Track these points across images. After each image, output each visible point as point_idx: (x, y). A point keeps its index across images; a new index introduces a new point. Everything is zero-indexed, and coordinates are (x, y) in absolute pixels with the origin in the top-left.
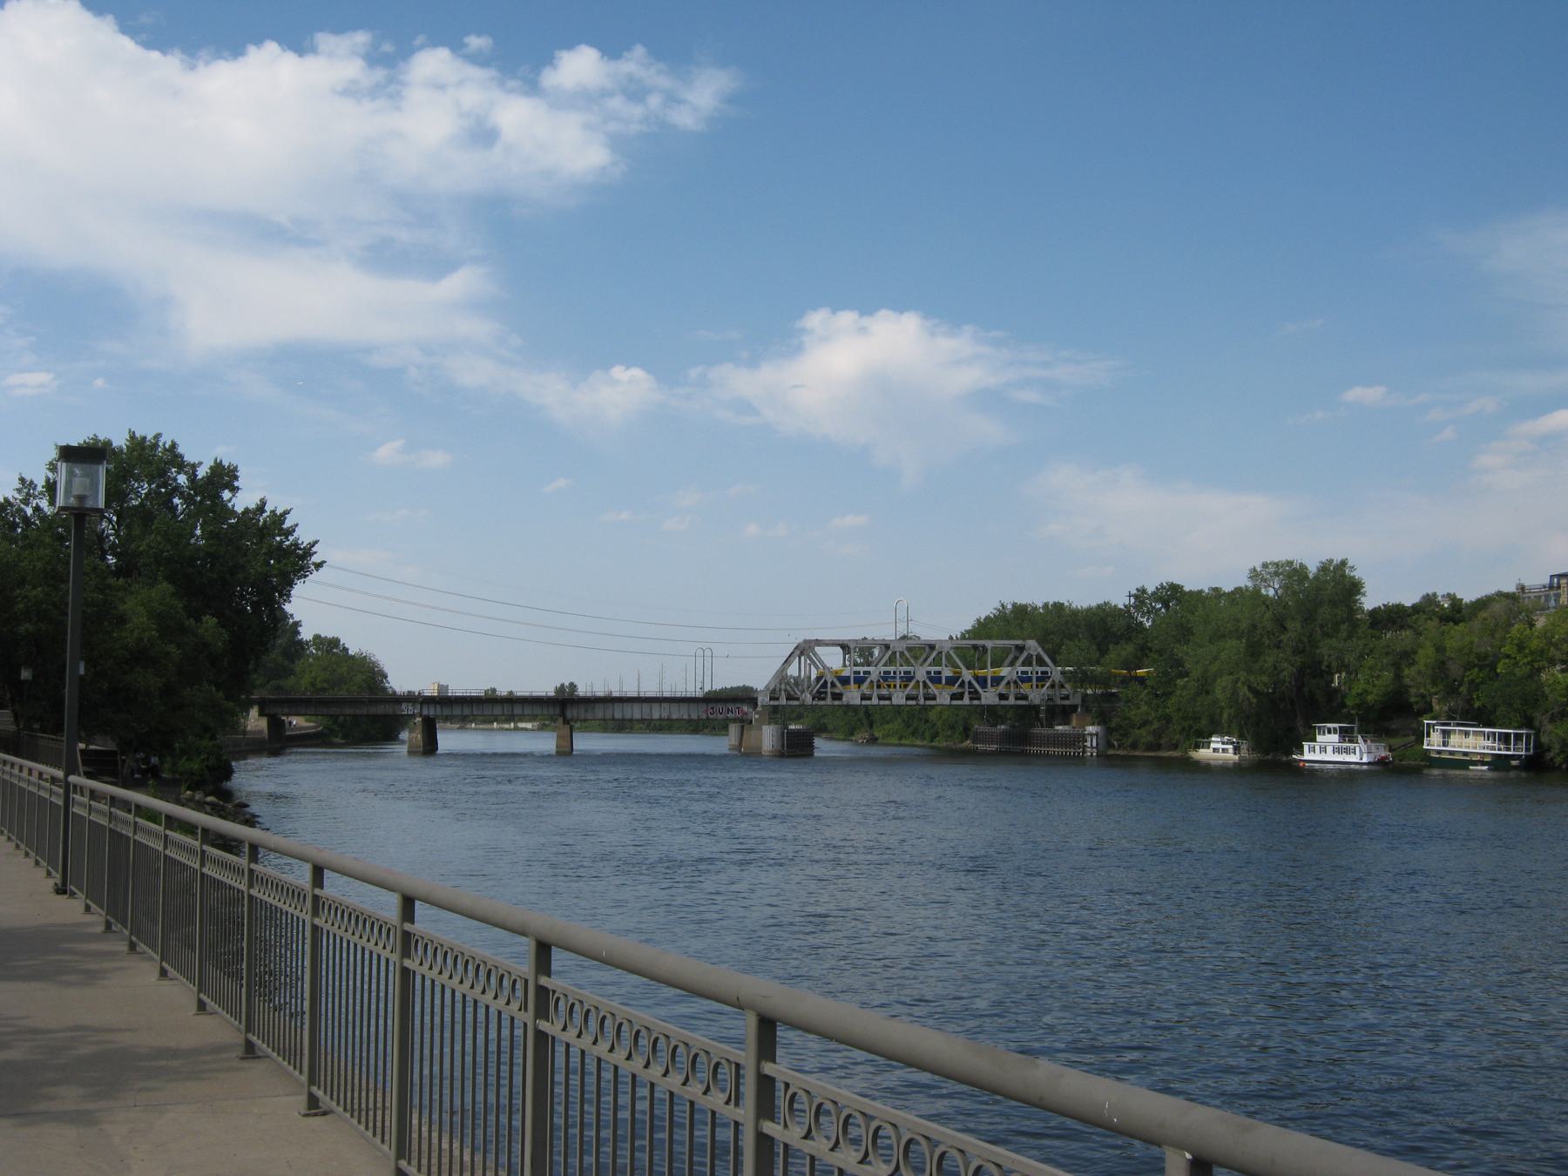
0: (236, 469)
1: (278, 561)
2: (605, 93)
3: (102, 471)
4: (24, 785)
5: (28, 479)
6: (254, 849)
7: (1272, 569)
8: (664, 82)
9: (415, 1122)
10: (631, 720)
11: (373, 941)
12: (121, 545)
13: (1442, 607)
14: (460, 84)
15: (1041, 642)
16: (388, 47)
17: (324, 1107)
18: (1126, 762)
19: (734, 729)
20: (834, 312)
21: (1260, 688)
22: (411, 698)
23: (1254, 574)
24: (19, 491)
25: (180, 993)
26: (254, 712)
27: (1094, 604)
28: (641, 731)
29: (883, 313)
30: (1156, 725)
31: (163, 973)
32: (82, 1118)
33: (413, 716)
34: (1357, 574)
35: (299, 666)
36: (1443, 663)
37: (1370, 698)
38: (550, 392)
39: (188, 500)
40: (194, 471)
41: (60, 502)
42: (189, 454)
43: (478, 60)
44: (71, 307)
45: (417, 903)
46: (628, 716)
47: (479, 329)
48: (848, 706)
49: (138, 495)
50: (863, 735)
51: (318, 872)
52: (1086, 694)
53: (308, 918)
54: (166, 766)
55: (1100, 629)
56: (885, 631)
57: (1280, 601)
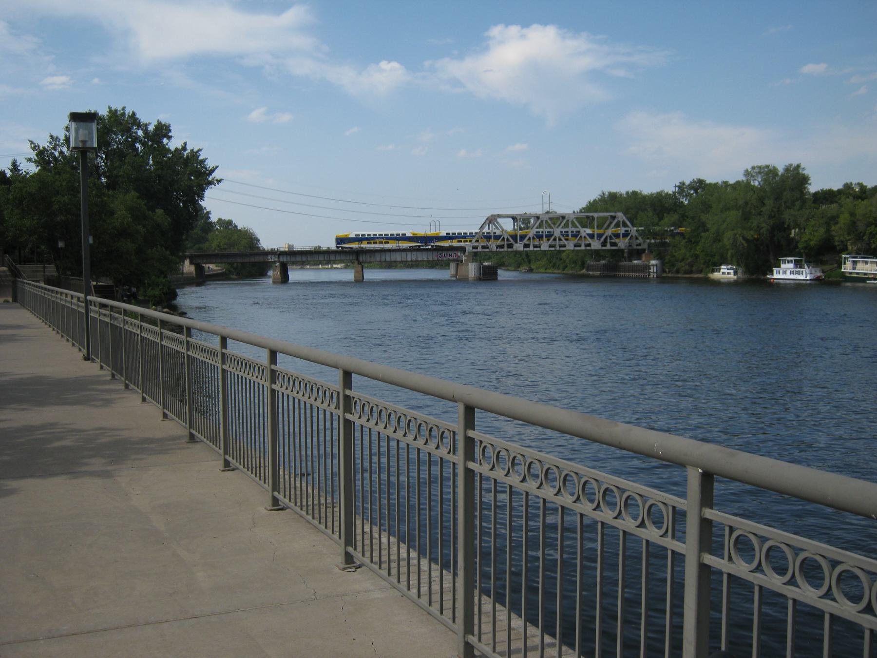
0: (169, 126)
1: (196, 178)
3: (94, 126)
4: (63, 303)
5: (55, 136)
6: (189, 329)
7: (757, 170)
9: (282, 473)
10: (395, 262)
11: (255, 376)
12: (109, 171)
13: (855, 192)
15: (625, 214)
17: (233, 467)
18: (673, 280)
19: (453, 265)
20: (507, 26)
21: (749, 237)
22: (273, 252)
23: (747, 173)
24: (50, 143)
25: (153, 410)
26: (187, 262)
28: (401, 268)
29: (535, 26)
30: (690, 260)
31: (144, 400)
33: (275, 262)
34: (806, 172)
35: (210, 236)
36: (854, 223)
37: (812, 243)
38: (345, 76)
39: (144, 144)
40: (147, 129)
41: (72, 144)
42: (143, 118)
45: (278, 354)
46: (394, 259)
48: (516, 251)
50: (524, 268)
51: (224, 340)
52: (651, 241)
53: (219, 365)
55: (658, 206)
57: (761, 189)
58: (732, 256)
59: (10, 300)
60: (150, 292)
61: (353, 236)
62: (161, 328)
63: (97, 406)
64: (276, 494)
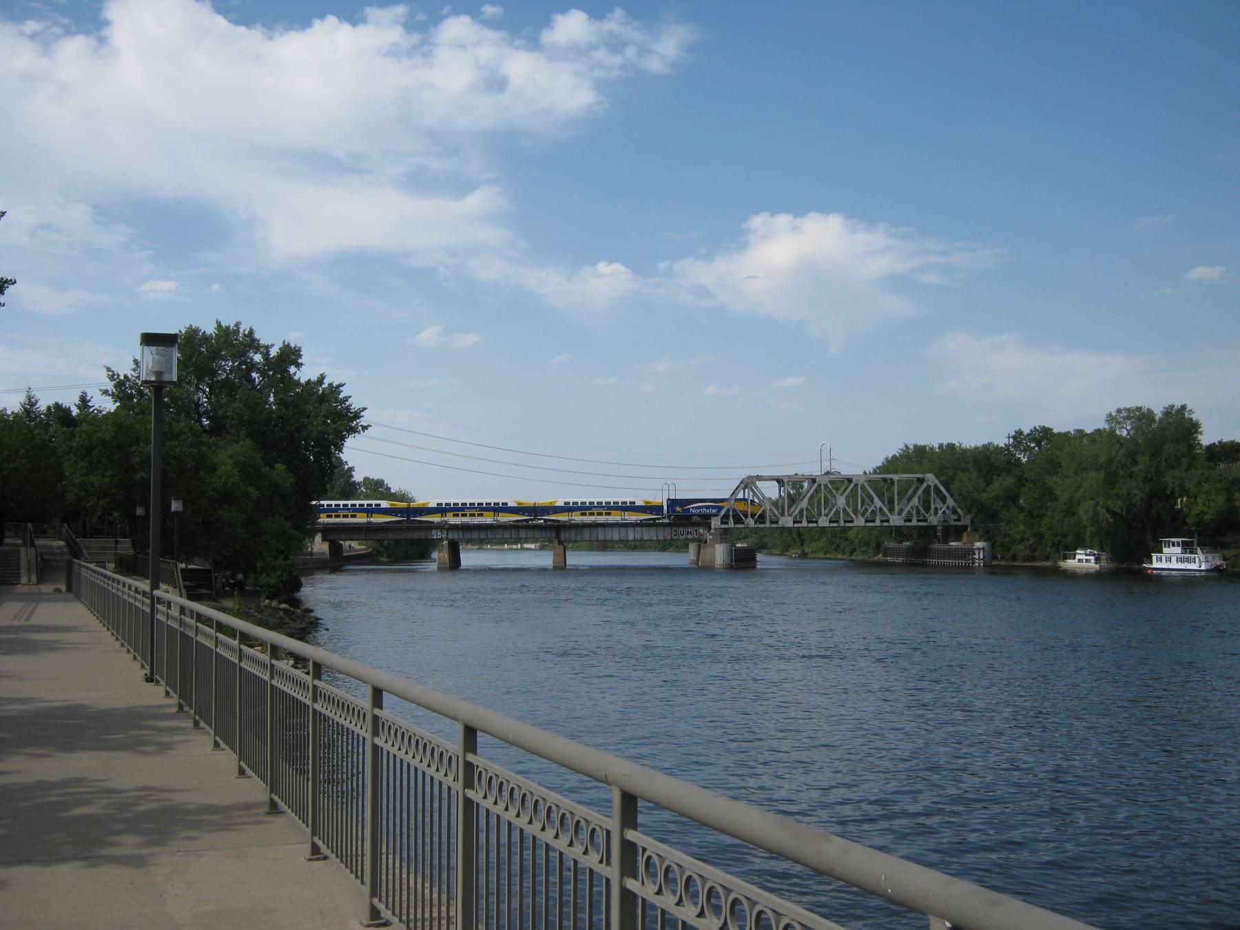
0: (299, 350)
1: (334, 422)
2: (592, 47)
4: (126, 597)
7: (1124, 414)
8: (638, 36)
10: (612, 541)
14: (478, 43)
16: (421, 17)
18: (1009, 571)
19: (692, 547)
20: (773, 215)
21: (1117, 509)
23: (1110, 418)
25: (228, 759)
26: (318, 538)
27: (980, 444)
28: (620, 550)
29: (811, 215)
30: (1032, 541)
31: (217, 745)
32: (137, 862)
33: (442, 539)
34: (1194, 417)
37: (1207, 517)
38: (549, 283)
39: (263, 373)
40: (268, 354)
42: (263, 337)
43: (492, 24)
44: (179, 226)
46: (609, 538)
47: (493, 235)
48: (783, 528)
49: (225, 371)
52: (976, 514)
54: (250, 581)
55: (987, 462)
56: (812, 468)
57: (1132, 440)
58: (1092, 537)
59: (63, 587)
60: (264, 580)
61: (560, 503)
62: (240, 643)
63: (145, 753)
64: (376, 901)
